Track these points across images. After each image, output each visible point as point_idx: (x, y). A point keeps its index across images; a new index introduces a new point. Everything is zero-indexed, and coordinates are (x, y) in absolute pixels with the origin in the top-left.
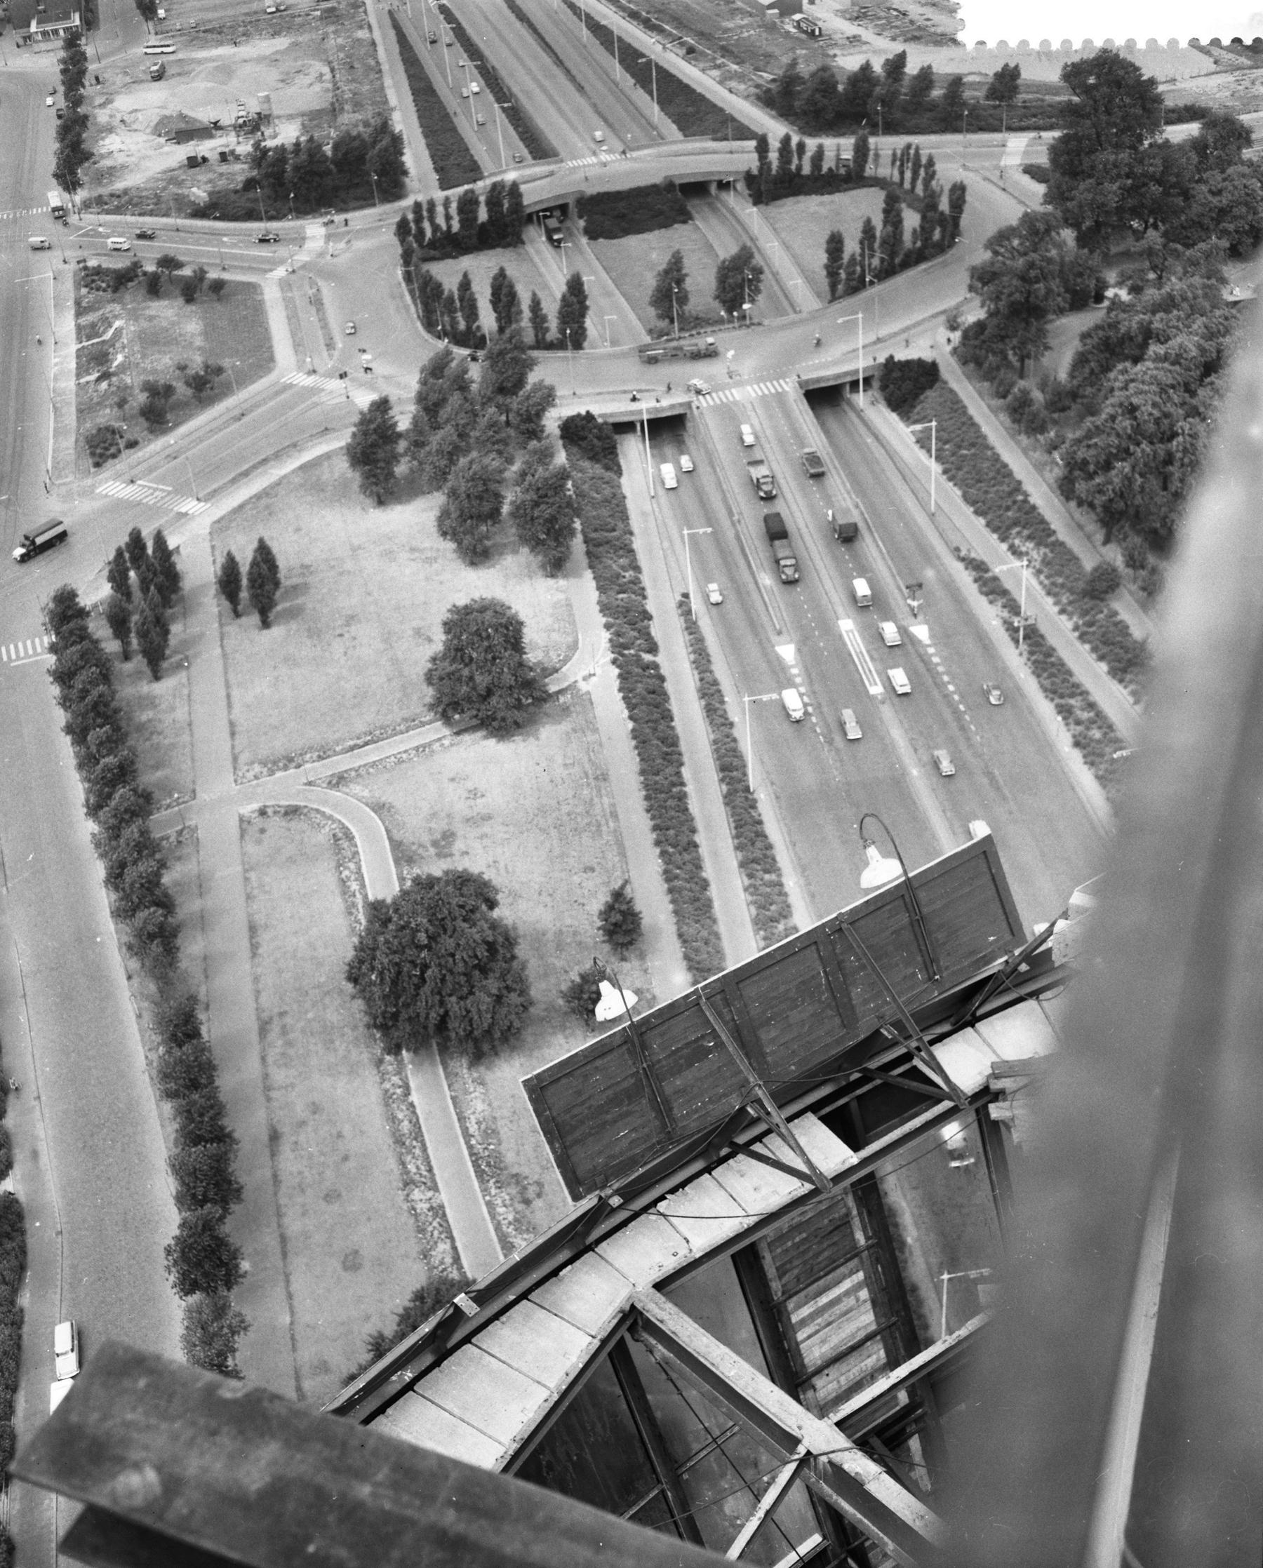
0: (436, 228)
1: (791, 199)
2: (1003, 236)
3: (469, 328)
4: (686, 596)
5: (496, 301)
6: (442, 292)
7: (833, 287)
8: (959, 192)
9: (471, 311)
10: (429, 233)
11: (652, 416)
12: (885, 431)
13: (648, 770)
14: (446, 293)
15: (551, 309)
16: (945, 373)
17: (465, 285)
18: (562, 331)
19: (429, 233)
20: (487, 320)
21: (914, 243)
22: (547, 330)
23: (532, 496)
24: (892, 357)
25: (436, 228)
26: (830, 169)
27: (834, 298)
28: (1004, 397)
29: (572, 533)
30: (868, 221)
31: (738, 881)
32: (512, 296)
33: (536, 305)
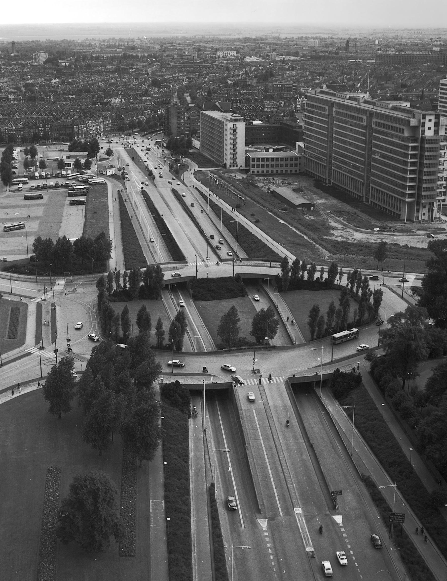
0: (118, 285)
1: (298, 291)
2: (399, 316)
3: (124, 335)
4: (212, 485)
5: (139, 323)
6: (112, 316)
7: (312, 332)
8: (379, 295)
9: (126, 326)
10: (115, 288)
12: (330, 408)
13: (12, 360)
14: (115, 316)
15: (166, 327)
16: (364, 380)
17: (125, 312)
18: (170, 340)
19: (115, 288)
21: (355, 317)
22: (164, 339)
24: (338, 370)
25: (118, 285)
26: (318, 278)
27: (312, 339)
29: (156, 445)
30: (332, 304)
31: (427, 194)
32: (148, 320)
33: (159, 326)
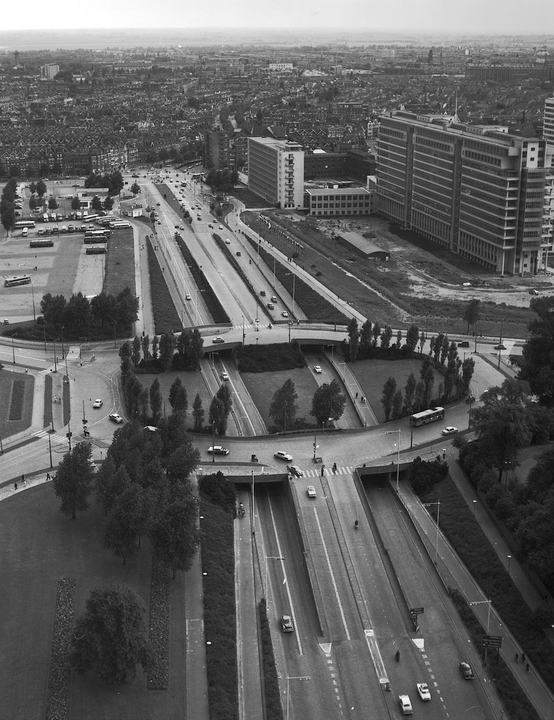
0: (147, 354)
1: (369, 360)
2: (494, 391)
3: (154, 415)
4: (263, 601)
5: (172, 400)
6: (139, 391)
7: (387, 412)
8: (469, 365)
9: (156, 404)
10: (142, 357)
11: (258, 481)
12: (409, 506)
14: (143, 392)
15: (206, 405)
16: (451, 471)
17: (155, 387)
18: (211, 422)
19: (142, 357)
20: (167, 410)
21: (440, 392)
22: (203, 420)
23: (342, 642)
24: (419, 459)
25: (147, 354)
26: (394, 345)
27: (387, 420)
28: (500, 161)
29: (193, 552)
30: (412, 377)
32: (183, 397)
33: (197, 404)
